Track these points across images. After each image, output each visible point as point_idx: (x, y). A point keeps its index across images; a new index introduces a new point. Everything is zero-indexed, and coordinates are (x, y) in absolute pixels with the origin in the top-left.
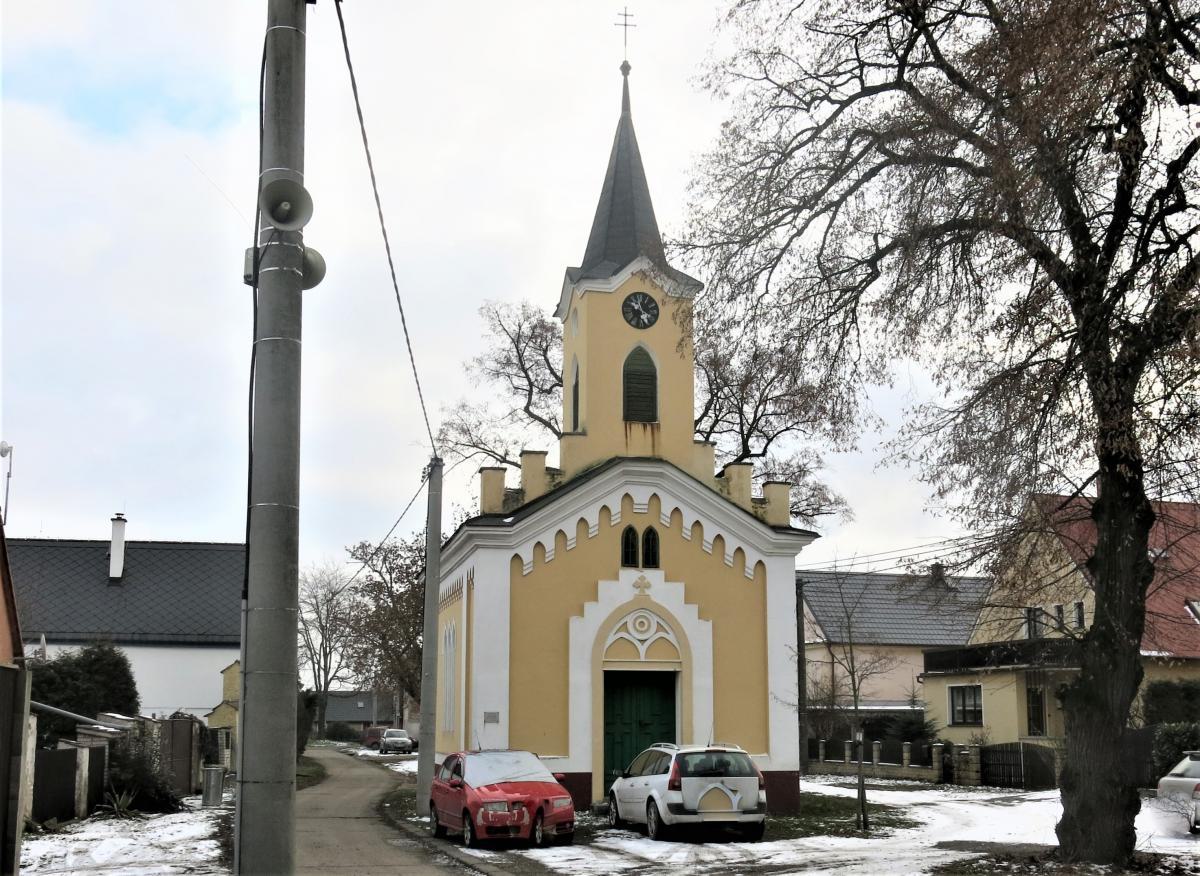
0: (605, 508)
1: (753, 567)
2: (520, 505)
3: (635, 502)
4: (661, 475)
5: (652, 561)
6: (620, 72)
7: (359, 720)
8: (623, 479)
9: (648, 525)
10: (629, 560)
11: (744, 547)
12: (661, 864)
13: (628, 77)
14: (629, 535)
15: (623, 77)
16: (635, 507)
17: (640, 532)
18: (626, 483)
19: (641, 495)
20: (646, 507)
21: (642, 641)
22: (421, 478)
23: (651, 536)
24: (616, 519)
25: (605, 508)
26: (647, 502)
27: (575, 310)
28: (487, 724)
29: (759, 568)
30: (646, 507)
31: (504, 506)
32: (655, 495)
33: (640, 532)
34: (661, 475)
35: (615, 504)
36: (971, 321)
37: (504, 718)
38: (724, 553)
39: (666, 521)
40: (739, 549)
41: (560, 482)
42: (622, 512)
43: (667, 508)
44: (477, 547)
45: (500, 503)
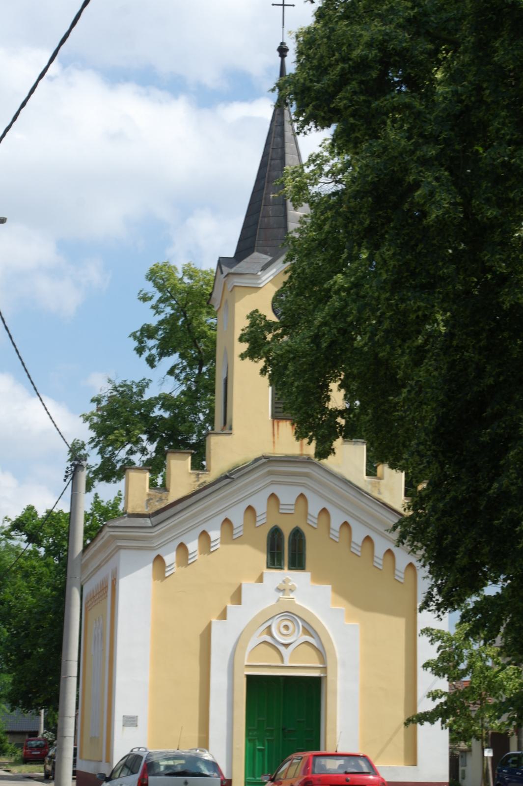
0: (250, 508)
1: (338, 529)
2: (163, 506)
3: (282, 502)
4: (306, 475)
5: (298, 562)
6: (278, 54)
7: (24, 730)
8: (269, 479)
9: (294, 526)
10: (274, 560)
11: (351, 522)
12: (113, 771)
13: (286, 59)
14: (275, 536)
15: (280, 59)
16: (281, 507)
17: (287, 533)
18: (273, 483)
19: (288, 496)
20: (293, 507)
21: (286, 645)
22: (63, 478)
23: (298, 536)
24: (261, 519)
25: (250, 508)
26: (293, 502)
27: (227, 301)
28: (127, 728)
29: (345, 530)
30: (293, 507)
31: (147, 507)
32: (302, 495)
33: (287, 533)
34: (306, 475)
35: (261, 504)
36: (355, 93)
37: (143, 721)
38: (394, 568)
39: (313, 521)
40: (346, 524)
41: (205, 482)
42: (267, 512)
43: (314, 508)
44: (120, 548)
45: (144, 504)
